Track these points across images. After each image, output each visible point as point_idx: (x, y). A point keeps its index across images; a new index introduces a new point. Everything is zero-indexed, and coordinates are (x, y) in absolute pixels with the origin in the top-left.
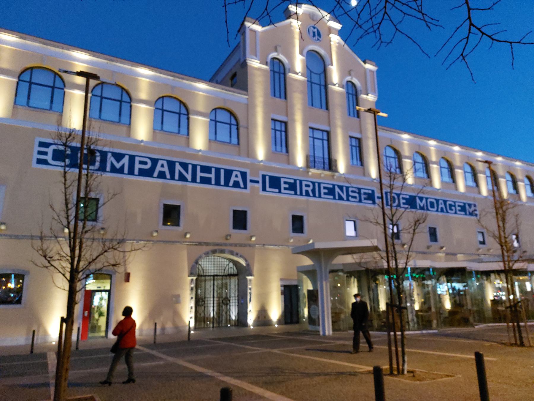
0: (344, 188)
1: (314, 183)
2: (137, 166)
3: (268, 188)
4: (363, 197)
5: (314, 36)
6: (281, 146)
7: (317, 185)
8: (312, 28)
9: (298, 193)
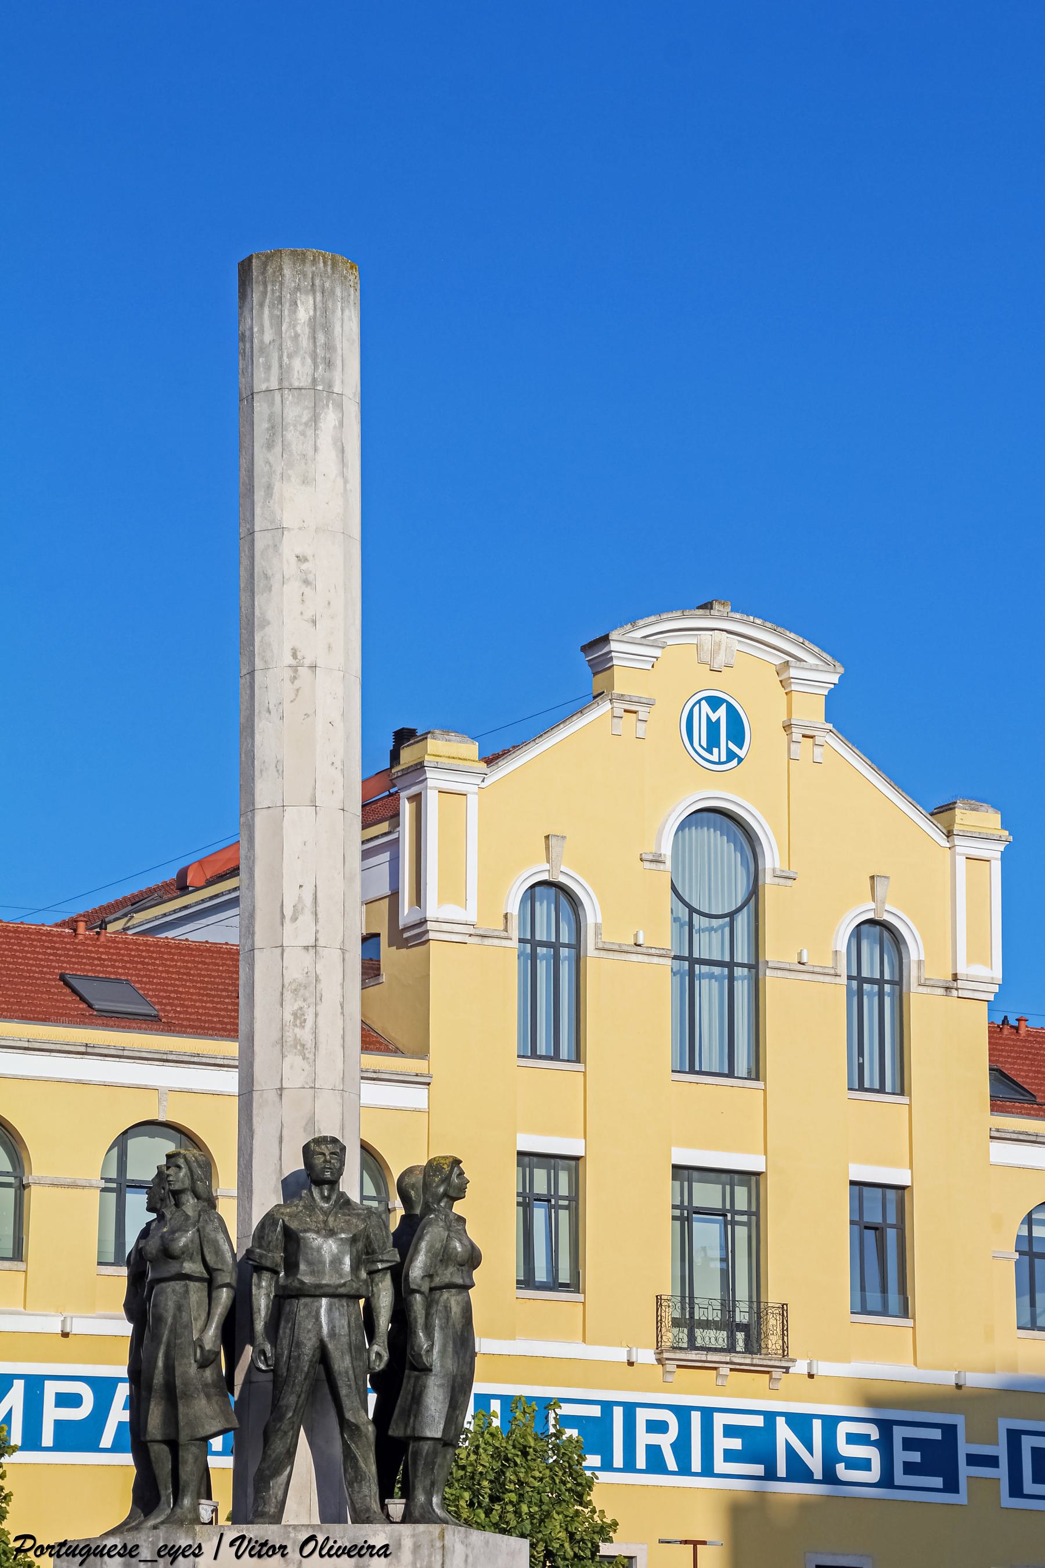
0: (817, 1425)
1: (682, 1413)
2: (51, 1414)
3: (1029, 1486)
4: (901, 1456)
5: (713, 741)
6: (884, 1290)
7: (696, 1417)
8: (705, 706)
9: (618, 1461)
